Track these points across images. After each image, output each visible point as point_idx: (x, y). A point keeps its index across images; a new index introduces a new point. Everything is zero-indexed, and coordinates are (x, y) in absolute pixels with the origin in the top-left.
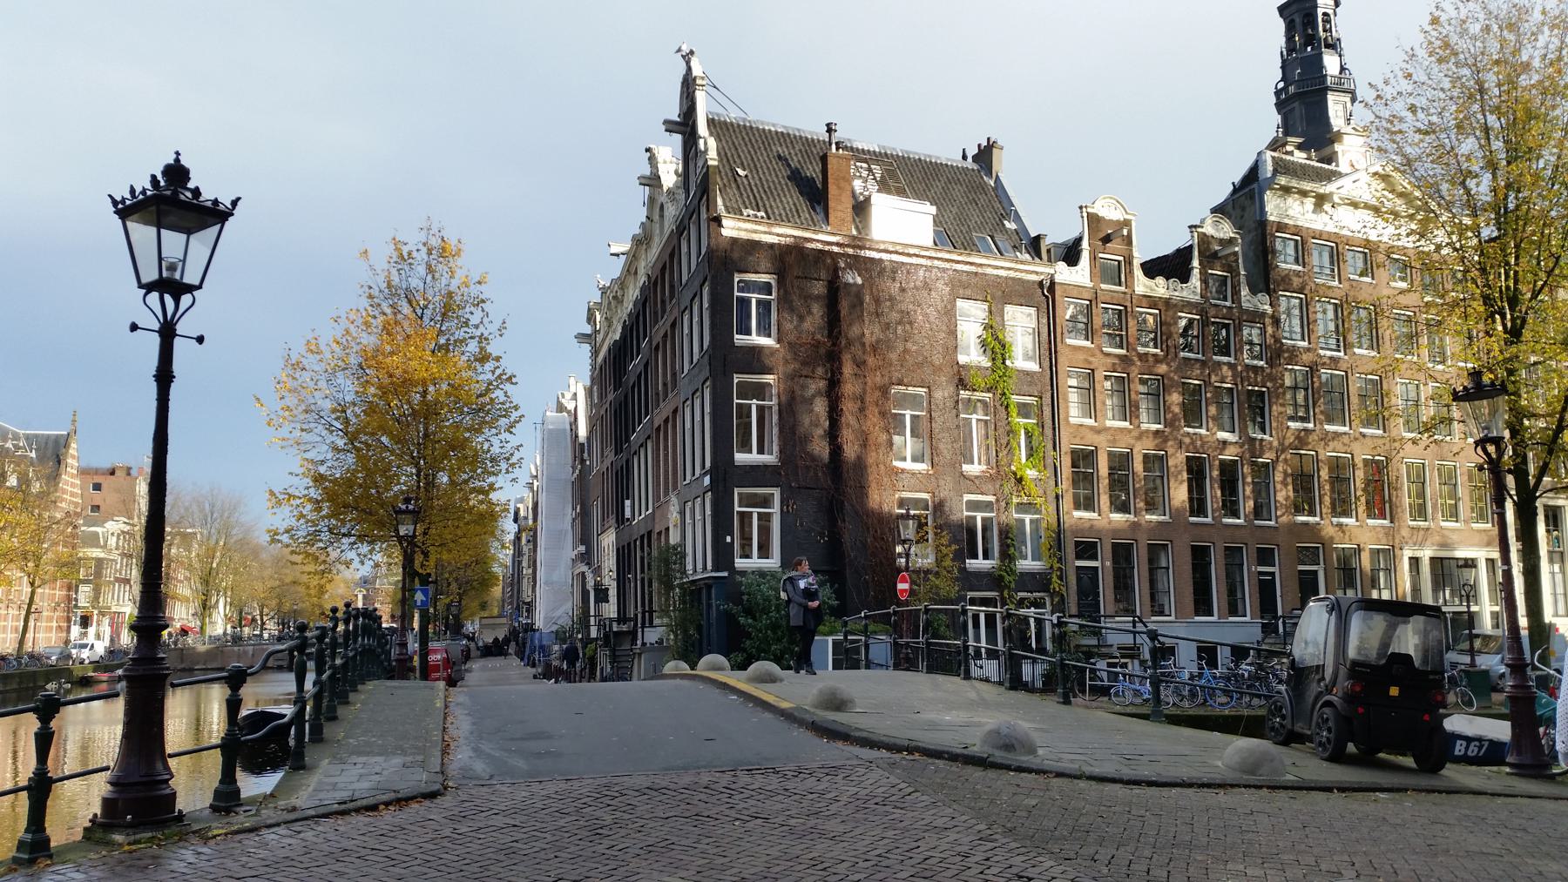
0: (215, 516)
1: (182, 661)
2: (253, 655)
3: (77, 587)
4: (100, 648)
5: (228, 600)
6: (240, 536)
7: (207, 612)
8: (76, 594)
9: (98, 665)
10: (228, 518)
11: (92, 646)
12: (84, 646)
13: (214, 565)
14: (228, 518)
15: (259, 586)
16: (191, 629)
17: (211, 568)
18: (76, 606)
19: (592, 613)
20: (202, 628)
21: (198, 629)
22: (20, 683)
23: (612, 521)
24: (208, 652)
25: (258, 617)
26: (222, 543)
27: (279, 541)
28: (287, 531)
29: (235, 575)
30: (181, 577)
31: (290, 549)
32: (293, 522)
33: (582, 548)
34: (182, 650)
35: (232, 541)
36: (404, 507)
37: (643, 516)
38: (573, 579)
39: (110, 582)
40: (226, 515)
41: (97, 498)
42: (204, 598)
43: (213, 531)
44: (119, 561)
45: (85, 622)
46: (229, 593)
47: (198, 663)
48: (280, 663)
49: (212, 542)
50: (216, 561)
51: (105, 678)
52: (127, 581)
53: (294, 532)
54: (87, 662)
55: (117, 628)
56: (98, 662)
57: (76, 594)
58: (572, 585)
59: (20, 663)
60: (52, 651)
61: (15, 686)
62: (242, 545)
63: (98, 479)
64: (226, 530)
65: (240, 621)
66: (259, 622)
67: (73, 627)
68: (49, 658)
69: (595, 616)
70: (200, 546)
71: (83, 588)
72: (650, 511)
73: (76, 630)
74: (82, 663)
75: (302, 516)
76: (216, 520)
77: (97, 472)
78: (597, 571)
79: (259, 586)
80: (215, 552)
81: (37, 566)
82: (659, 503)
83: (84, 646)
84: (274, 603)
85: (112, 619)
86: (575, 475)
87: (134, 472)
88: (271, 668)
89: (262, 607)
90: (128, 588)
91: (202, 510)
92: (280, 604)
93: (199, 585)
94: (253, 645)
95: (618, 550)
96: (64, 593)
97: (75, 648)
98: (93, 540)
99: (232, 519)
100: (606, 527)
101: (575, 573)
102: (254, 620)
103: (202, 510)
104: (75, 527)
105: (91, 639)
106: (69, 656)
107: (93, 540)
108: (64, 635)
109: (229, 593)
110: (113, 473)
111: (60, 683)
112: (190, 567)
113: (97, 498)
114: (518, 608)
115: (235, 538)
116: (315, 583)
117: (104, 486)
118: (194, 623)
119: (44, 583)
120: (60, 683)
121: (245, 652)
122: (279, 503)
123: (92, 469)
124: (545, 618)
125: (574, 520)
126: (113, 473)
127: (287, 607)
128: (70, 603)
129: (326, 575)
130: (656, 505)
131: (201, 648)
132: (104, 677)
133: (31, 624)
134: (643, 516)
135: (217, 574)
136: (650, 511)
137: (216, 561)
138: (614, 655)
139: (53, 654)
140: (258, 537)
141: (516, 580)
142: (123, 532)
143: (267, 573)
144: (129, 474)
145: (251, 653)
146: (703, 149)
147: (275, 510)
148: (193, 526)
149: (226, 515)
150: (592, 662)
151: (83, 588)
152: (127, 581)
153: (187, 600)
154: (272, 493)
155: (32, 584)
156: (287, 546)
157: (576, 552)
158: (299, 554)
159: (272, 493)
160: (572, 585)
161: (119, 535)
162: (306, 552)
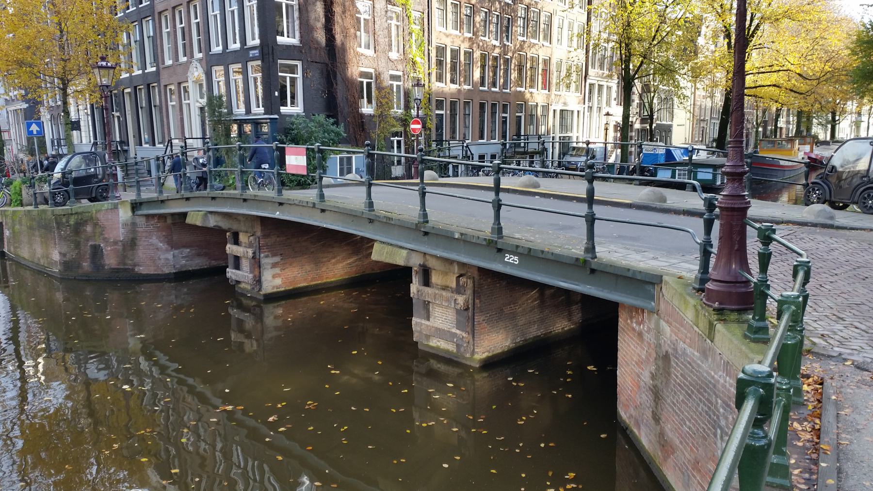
58: (8, 117)
160: (8, 117)
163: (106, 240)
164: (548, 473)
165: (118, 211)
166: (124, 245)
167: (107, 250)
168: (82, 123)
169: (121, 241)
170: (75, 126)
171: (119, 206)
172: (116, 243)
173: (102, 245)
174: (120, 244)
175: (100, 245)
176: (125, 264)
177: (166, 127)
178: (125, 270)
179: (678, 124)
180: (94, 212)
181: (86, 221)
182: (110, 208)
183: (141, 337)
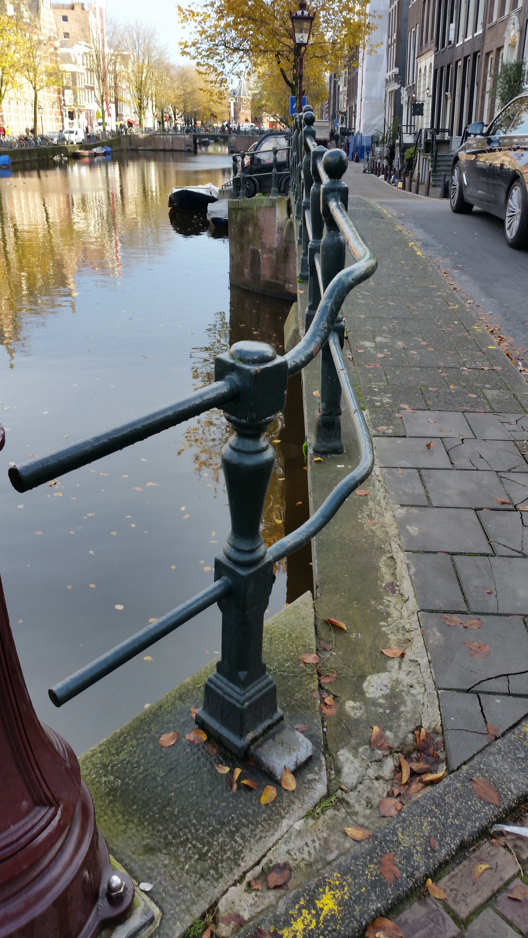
0: (140, 42)
1: (131, 144)
2: (172, 142)
3: (63, 92)
4: (81, 137)
5: (154, 103)
6: (157, 57)
7: (142, 111)
8: (63, 96)
9: (82, 145)
10: (149, 43)
11: (77, 132)
12: (72, 132)
13: (143, 79)
14: (149, 43)
15: (171, 94)
16: (134, 122)
17: (142, 80)
18: (65, 105)
19: (404, 123)
20: (140, 122)
21: (138, 123)
22: (39, 156)
23: (432, 45)
24: (145, 139)
25: (173, 116)
26: (146, 63)
27: (188, 53)
28: (194, 44)
29: (157, 86)
30: (124, 86)
31: (196, 61)
32: (198, 36)
33: (396, 70)
34: (130, 136)
35: (153, 61)
36: (299, 13)
37: (469, 37)
38: (386, 95)
39: (82, 89)
40: (147, 41)
41: (66, 27)
42: (139, 101)
43: (140, 53)
44: (86, 74)
45: (71, 116)
46: (154, 99)
47: (140, 146)
48: (189, 148)
49: (141, 61)
50: (144, 76)
51: (87, 154)
52: (92, 89)
53: (199, 45)
54: (75, 143)
55: (91, 121)
56: (81, 143)
57: (63, 96)
58: (385, 100)
59: (36, 142)
60: (54, 135)
61: (36, 158)
62: (159, 64)
63: (66, 13)
64: (148, 52)
65: (162, 117)
66: (173, 119)
67: (65, 119)
68: (52, 139)
69: (407, 126)
70: (133, 64)
71: (67, 92)
72: (480, 31)
73: (67, 120)
74: (72, 143)
75: (203, 32)
76: (141, 44)
77: (63, 7)
78: (413, 89)
79: (171, 94)
80: (142, 69)
81: (35, 75)
82: (491, 25)
83: (72, 132)
84: (181, 106)
85: (87, 114)
86: (393, 6)
87: (86, 7)
88: (372, 443)
89: (174, 109)
90: (93, 92)
91: (131, 37)
92: (185, 107)
93: (135, 92)
94: (172, 135)
95: (436, 71)
96: (56, 95)
97: (67, 133)
98: (67, 58)
99: (151, 45)
100: (424, 51)
101: (388, 91)
102: (170, 117)
103: (131, 37)
104: (56, 49)
105: (75, 128)
106: (64, 139)
107: (67, 58)
108: (61, 124)
109: (154, 99)
110: (73, 8)
111: (61, 157)
112: (129, 80)
113: (66, 27)
114: (334, 116)
115: (154, 59)
116: (217, 90)
117: (69, 18)
118: (135, 119)
119: (42, 88)
120: (61, 157)
121: (168, 140)
122: (185, 19)
123: (59, 5)
124: (365, 125)
125: (389, 46)
126: (73, 8)
127: (189, 109)
128: (61, 104)
129: (223, 84)
130: (488, 26)
131: (142, 136)
132: (86, 153)
133: (38, 116)
134: (469, 37)
135: (146, 84)
136: (480, 31)
137: (144, 76)
138: (436, 160)
139: (55, 137)
140: (169, 58)
141: (332, 96)
142: (85, 53)
143: (175, 85)
144: (83, 9)
145: (171, 140)
146: (145, 105)
147: (184, 24)
148: (127, 49)
149: (147, 41)
150: (410, 165)
151: (67, 92)
152: (92, 89)
153: (129, 102)
154: (180, 9)
155: (34, 88)
156: (194, 58)
157: (390, 73)
158: (203, 65)
159: (180, 9)
160: (385, 100)
161: (83, 55)
162: (208, 64)
163: (263, 245)
164: (94, 584)
165: (275, 210)
166: (277, 255)
167: (264, 256)
168: (425, 107)
169: (276, 249)
170: (418, 110)
171: (277, 204)
172: (270, 251)
173: (259, 251)
174: (274, 253)
175: (258, 251)
176: (277, 278)
177: (479, 107)
178: (277, 285)
179: (181, 6)
180: (255, 209)
181: (249, 220)
182: (268, 205)
183: (21, 283)
